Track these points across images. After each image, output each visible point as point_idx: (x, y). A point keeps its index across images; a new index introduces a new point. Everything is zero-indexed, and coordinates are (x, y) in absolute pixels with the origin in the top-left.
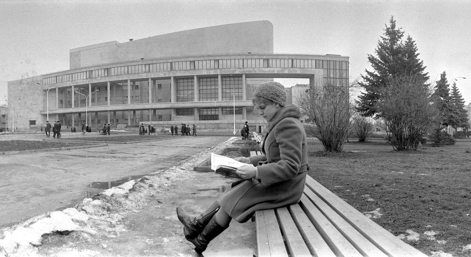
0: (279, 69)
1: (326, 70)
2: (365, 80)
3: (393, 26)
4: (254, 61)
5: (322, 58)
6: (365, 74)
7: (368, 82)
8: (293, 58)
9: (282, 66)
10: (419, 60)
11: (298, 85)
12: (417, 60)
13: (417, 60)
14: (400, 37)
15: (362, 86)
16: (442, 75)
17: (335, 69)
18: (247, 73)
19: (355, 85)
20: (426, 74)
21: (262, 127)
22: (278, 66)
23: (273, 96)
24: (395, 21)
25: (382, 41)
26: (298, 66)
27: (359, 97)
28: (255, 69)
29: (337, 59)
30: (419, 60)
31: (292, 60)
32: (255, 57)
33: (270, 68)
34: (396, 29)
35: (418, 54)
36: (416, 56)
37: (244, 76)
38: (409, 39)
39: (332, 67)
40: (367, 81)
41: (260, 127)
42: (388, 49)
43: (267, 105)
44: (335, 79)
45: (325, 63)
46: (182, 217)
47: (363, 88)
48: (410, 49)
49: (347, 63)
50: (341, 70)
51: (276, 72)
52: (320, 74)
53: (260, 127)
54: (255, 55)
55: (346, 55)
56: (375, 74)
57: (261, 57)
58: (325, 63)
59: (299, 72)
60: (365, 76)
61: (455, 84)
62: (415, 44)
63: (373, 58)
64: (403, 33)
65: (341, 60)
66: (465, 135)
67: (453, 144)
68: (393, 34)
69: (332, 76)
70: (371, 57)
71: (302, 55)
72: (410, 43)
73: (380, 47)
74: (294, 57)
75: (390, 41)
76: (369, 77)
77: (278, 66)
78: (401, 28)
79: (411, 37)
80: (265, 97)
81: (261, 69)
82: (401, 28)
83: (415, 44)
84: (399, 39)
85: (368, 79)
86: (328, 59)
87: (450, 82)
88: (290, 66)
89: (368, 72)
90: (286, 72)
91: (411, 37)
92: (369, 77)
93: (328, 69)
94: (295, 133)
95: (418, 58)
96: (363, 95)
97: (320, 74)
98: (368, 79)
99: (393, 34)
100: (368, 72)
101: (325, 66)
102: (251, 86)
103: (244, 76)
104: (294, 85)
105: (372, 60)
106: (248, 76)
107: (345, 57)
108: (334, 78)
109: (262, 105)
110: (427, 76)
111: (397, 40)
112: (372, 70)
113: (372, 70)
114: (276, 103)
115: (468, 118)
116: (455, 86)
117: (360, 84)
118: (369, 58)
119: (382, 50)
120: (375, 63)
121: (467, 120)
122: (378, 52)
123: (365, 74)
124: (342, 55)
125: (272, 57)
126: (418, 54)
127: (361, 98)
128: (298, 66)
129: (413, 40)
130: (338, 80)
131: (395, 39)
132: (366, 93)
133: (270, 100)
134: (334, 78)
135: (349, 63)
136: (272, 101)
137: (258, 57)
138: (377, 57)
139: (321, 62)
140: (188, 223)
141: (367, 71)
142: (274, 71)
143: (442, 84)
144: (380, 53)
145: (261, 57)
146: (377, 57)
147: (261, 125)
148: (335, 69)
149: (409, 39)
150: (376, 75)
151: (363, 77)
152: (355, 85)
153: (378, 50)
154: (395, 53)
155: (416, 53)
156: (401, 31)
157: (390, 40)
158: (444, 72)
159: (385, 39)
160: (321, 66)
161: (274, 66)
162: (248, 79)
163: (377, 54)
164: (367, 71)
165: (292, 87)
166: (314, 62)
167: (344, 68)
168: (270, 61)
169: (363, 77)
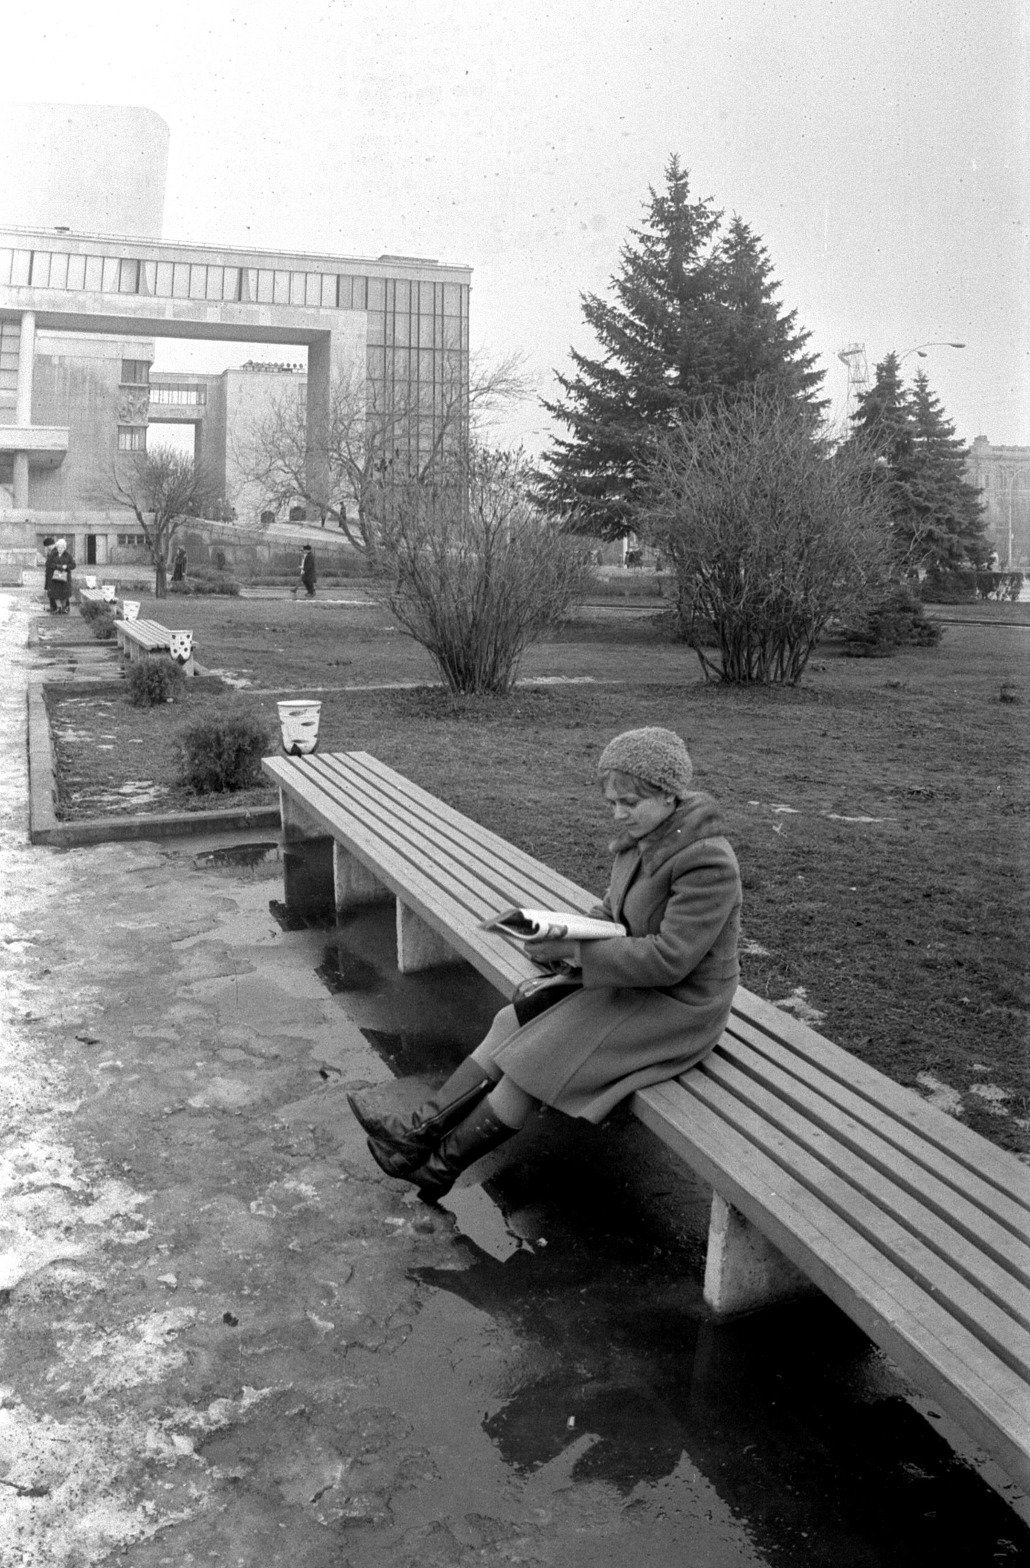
0: (185, 303)
1: (378, 318)
2: (573, 393)
3: (679, 193)
4: (77, 263)
5: (363, 271)
6: (573, 372)
7: (585, 401)
8: (243, 267)
9: (197, 292)
10: (780, 305)
11: (253, 367)
12: (773, 309)
13: (773, 309)
14: (706, 231)
15: (558, 416)
16: (880, 368)
17: (414, 314)
18: (45, 308)
19: (503, 386)
20: (807, 362)
21: (100, 541)
22: (180, 290)
23: (666, 775)
24: (686, 174)
25: (640, 249)
26: (265, 296)
27: (545, 457)
28: (81, 297)
29: (426, 276)
30: (780, 305)
31: (241, 271)
32: (83, 248)
33: (146, 294)
34: (691, 201)
35: (774, 285)
36: (767, 292)
37: (29, 322)
38: (739, 230)
39: (402, 306)
40: (581, 397)
41: (91, 540)
42: (663, 275)
43: (645, 797)
44: (414, 352)
45: (376, 288)
46: (377, 1122)
47: (562, 424)
48: (745, 269)
49: (464, 288)
50: (438, 316)
51: (168, 316)
52: (351, 335)
53: (91, 540)
54: (87, 240)
55: (460, 262)
56: (609, 366)
57: (112, 250)
58: (376, 288)
59: (265, 318)
60: (571, 378)
61: (923, 380)
62: (763, 250)
63: (602, 306)
64: (721, 214)
65: (441, 277)
66: (970, 587)
67: (930, 644)
68: (678, 219)
69: (401, 338)
70: (594, 304)
71: (281, 256)
72: (743, 244)
73: (630, 269)
74: (246, 262)
75: (668, 245)
76: (588, 381)
77: (180, 290)
78: (711, 199)
79: (744, 223)
80: (643, 777)
81: (107, 297)
82: (711, 199)
83: (763, 250)
84: (705, 239)
85: (583, 391)
86: (390, 273)
87: (906, 377)
88: (230, 293)
89: (582, 361)
90: (212, 316)
91: (744, 223)
92: (588, 381)
93: (388, 314)
94: (720, 881)
95: (774, 298)
96: (563, 450)
97: (351, 335)
98: (583, 391)
99: (678, 219)
100: (582, 361)
101: (376, 302)
102: (55, 361)
103: (29, 322)
104: (237, 365)
105: (596, 314)
106: (45, 321)
107: (455, 270)
108: (410, 348)
109: (631, 796)
110: (815, 368)
111: (697, 243)
112: (597, 352)
113: (597, 352)
114: (667, 794)
115: (983, 517)
116: (922, 388)
117: (550, 408)
118: (586, 307)
119: (643, 278)
120: (610, 327)
121: (980, 527)
122: (624, 290)
123: (573, 372)
124: (445, 259)
125: (155, 255)
126: (774, 285)
127: (557, 463)
128: (265, 296)
129: (752, 235)
130: (426, 358)
131: (688, 236)
132: (576, 442)
133: (654, 786)
134: (410, 348)
135: (469, 289)
136: (659, 788)
137: (98, 250)
138: (614, 301)
139: (359, 284)
140: (399, 1136)
141: (576, 356)
142: (161, 311)
143: (880, 404)
144: (630, 293)
145: (112, 250)
146: (614, 301)
147: (95, 531)
148: (414, 314)
149: (739, 230)
150: (615, 374)
151: (562, 380)
152: (503, 386)
153: (622, 277)
154: (688, 288)
155: (766, 281)
156: (710, 207)
157: (668, 241)
158: (892, 358)
159: (649, 238)
160: (359, 301)
161: (163, 289)
162: (41, 332)
163: (617, 292)
164: (576, 356)
165: (225, 373)
166: (330, 282)
167: (451, 309)
168: (149, 269)
169: (562, 380)
